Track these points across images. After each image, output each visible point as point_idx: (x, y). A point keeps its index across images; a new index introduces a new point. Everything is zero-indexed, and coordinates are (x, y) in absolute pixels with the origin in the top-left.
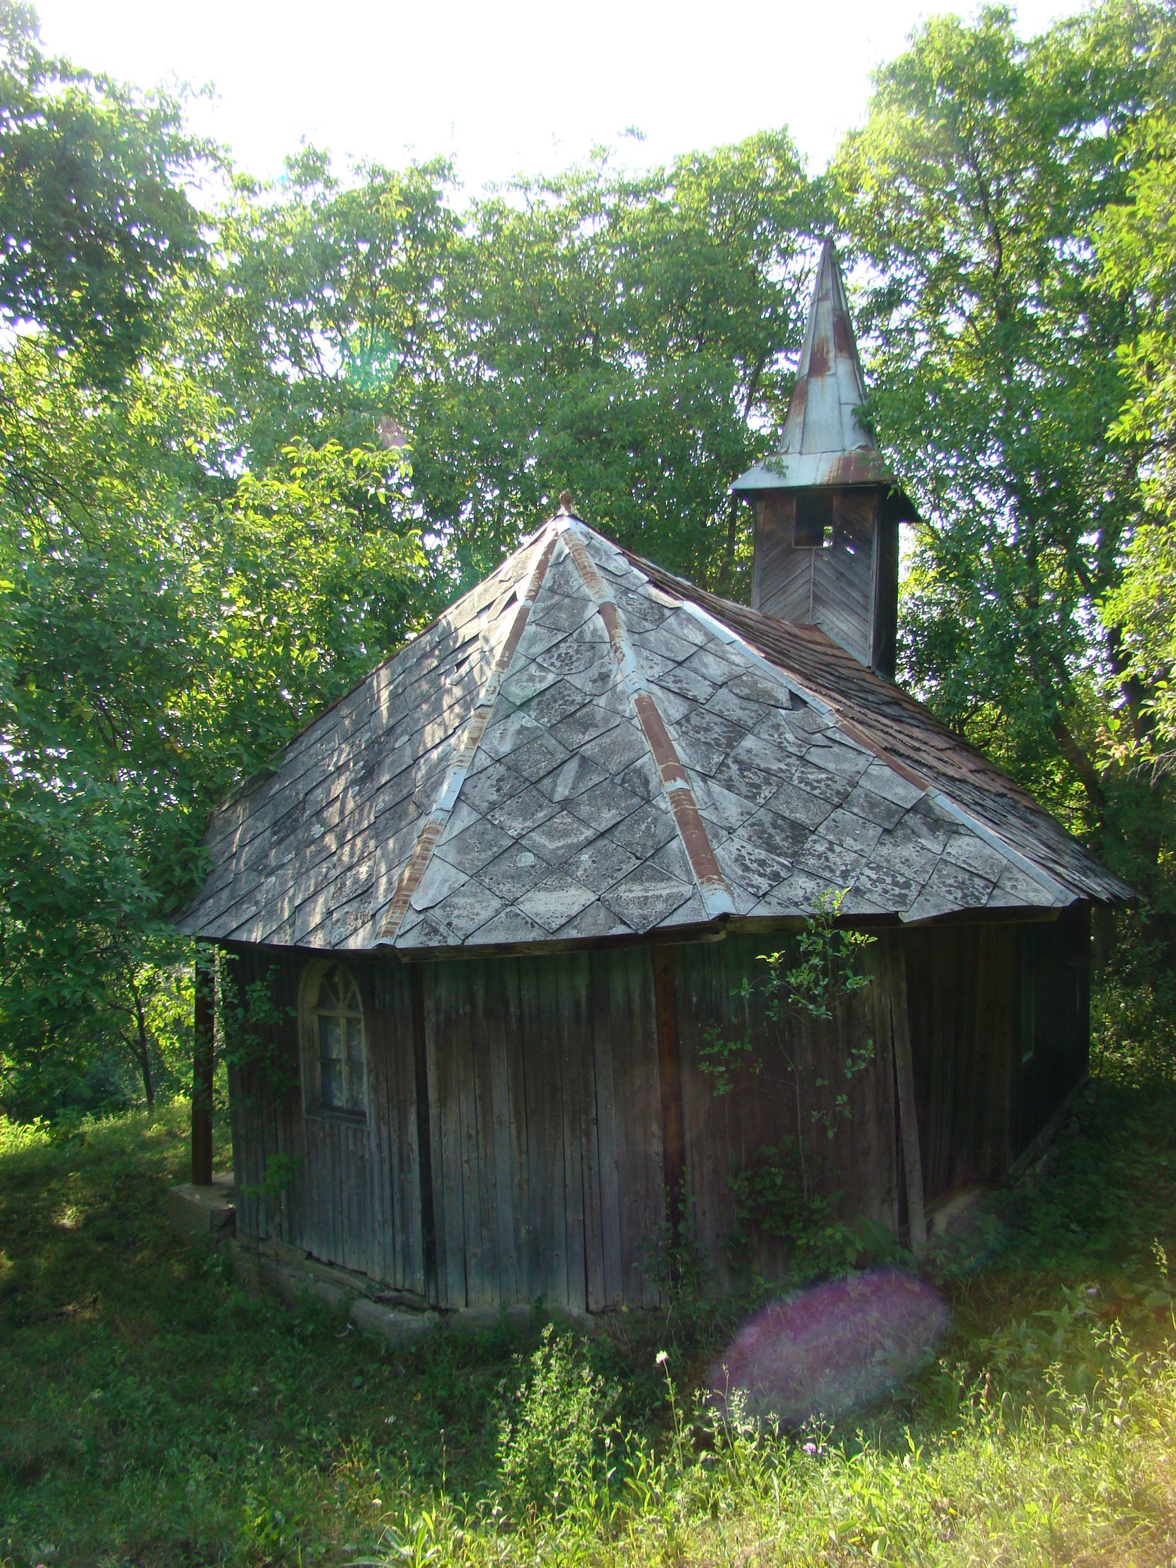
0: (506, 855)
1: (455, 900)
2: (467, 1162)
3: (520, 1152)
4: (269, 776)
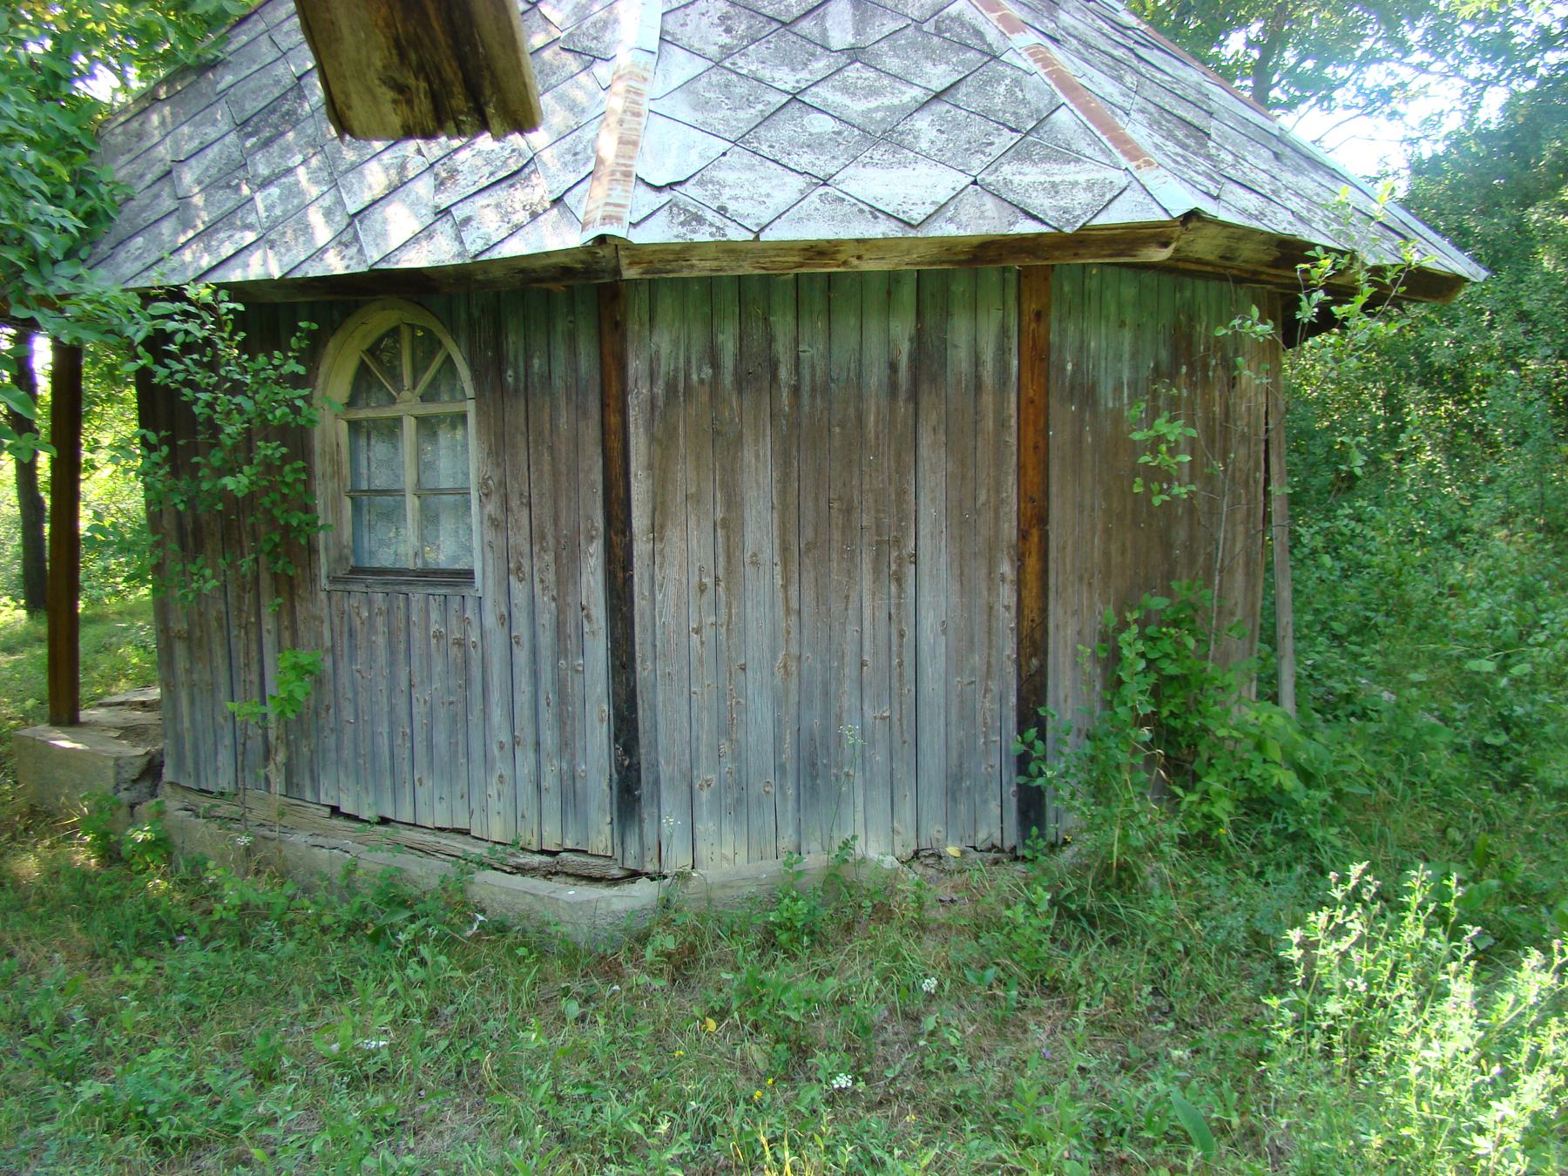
0: (780, 115)
1: (719, 175)
2: (698, 631)
3: (788, 611)
4: (208, 66)
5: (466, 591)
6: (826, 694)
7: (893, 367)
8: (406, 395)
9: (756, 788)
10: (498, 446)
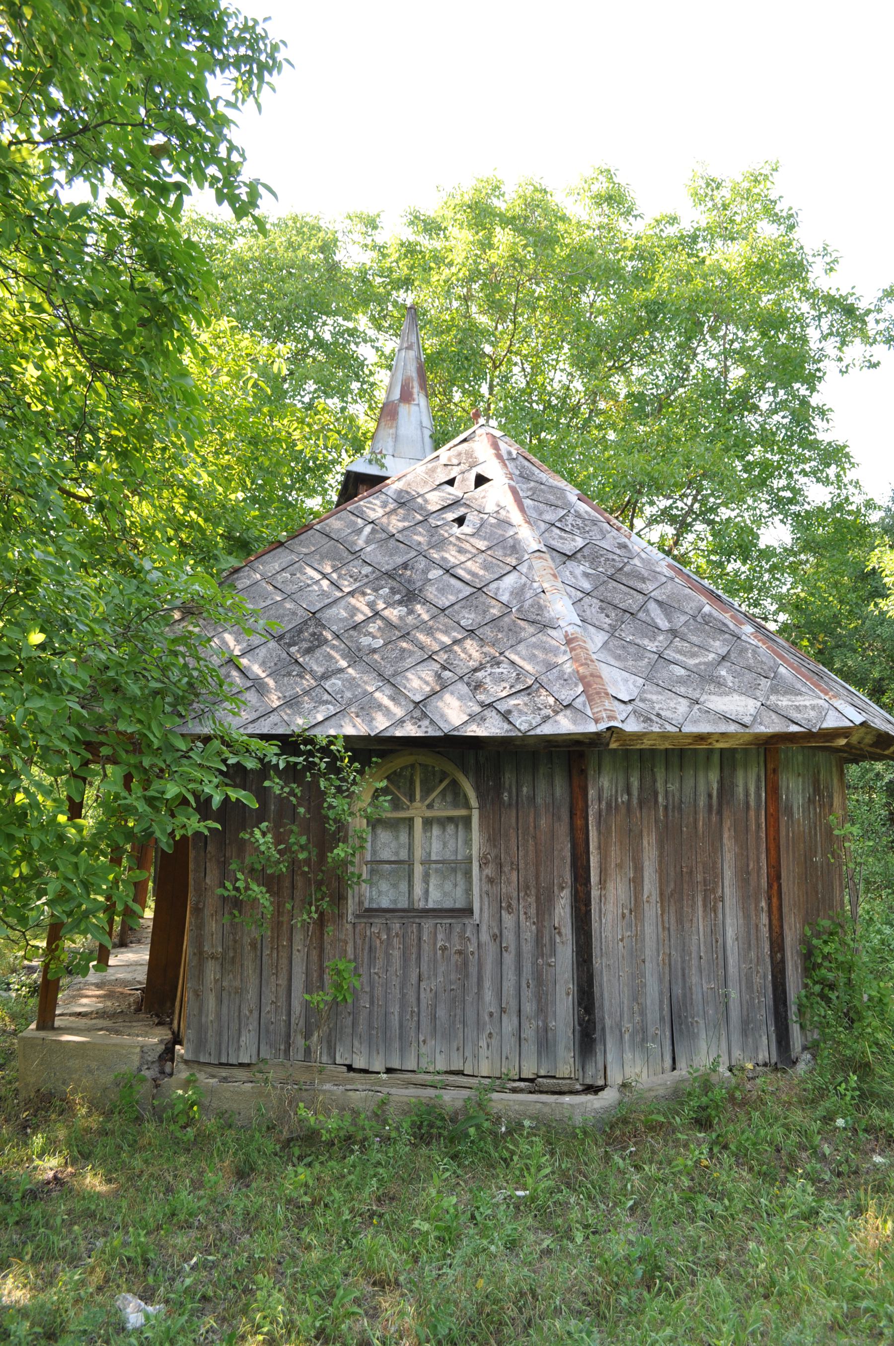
5: (466, 921)
6: (684, 975)
7: (710, 796)
8: (417, 804)
9: (651, 1030)
10: (493, 837)
